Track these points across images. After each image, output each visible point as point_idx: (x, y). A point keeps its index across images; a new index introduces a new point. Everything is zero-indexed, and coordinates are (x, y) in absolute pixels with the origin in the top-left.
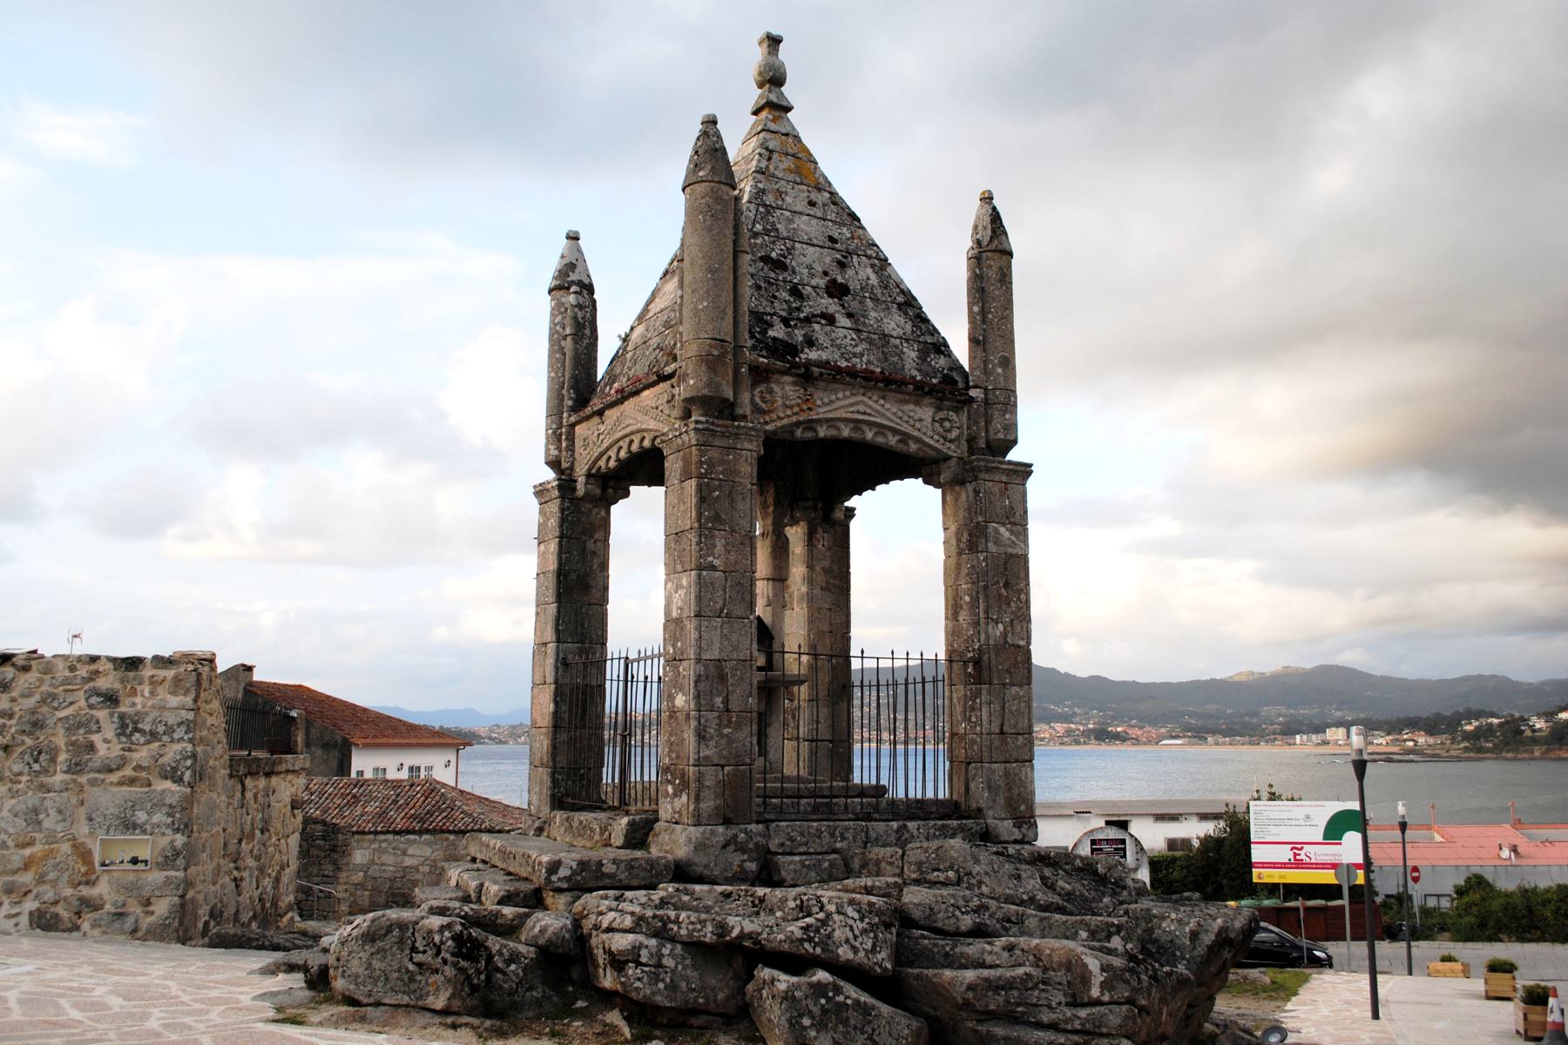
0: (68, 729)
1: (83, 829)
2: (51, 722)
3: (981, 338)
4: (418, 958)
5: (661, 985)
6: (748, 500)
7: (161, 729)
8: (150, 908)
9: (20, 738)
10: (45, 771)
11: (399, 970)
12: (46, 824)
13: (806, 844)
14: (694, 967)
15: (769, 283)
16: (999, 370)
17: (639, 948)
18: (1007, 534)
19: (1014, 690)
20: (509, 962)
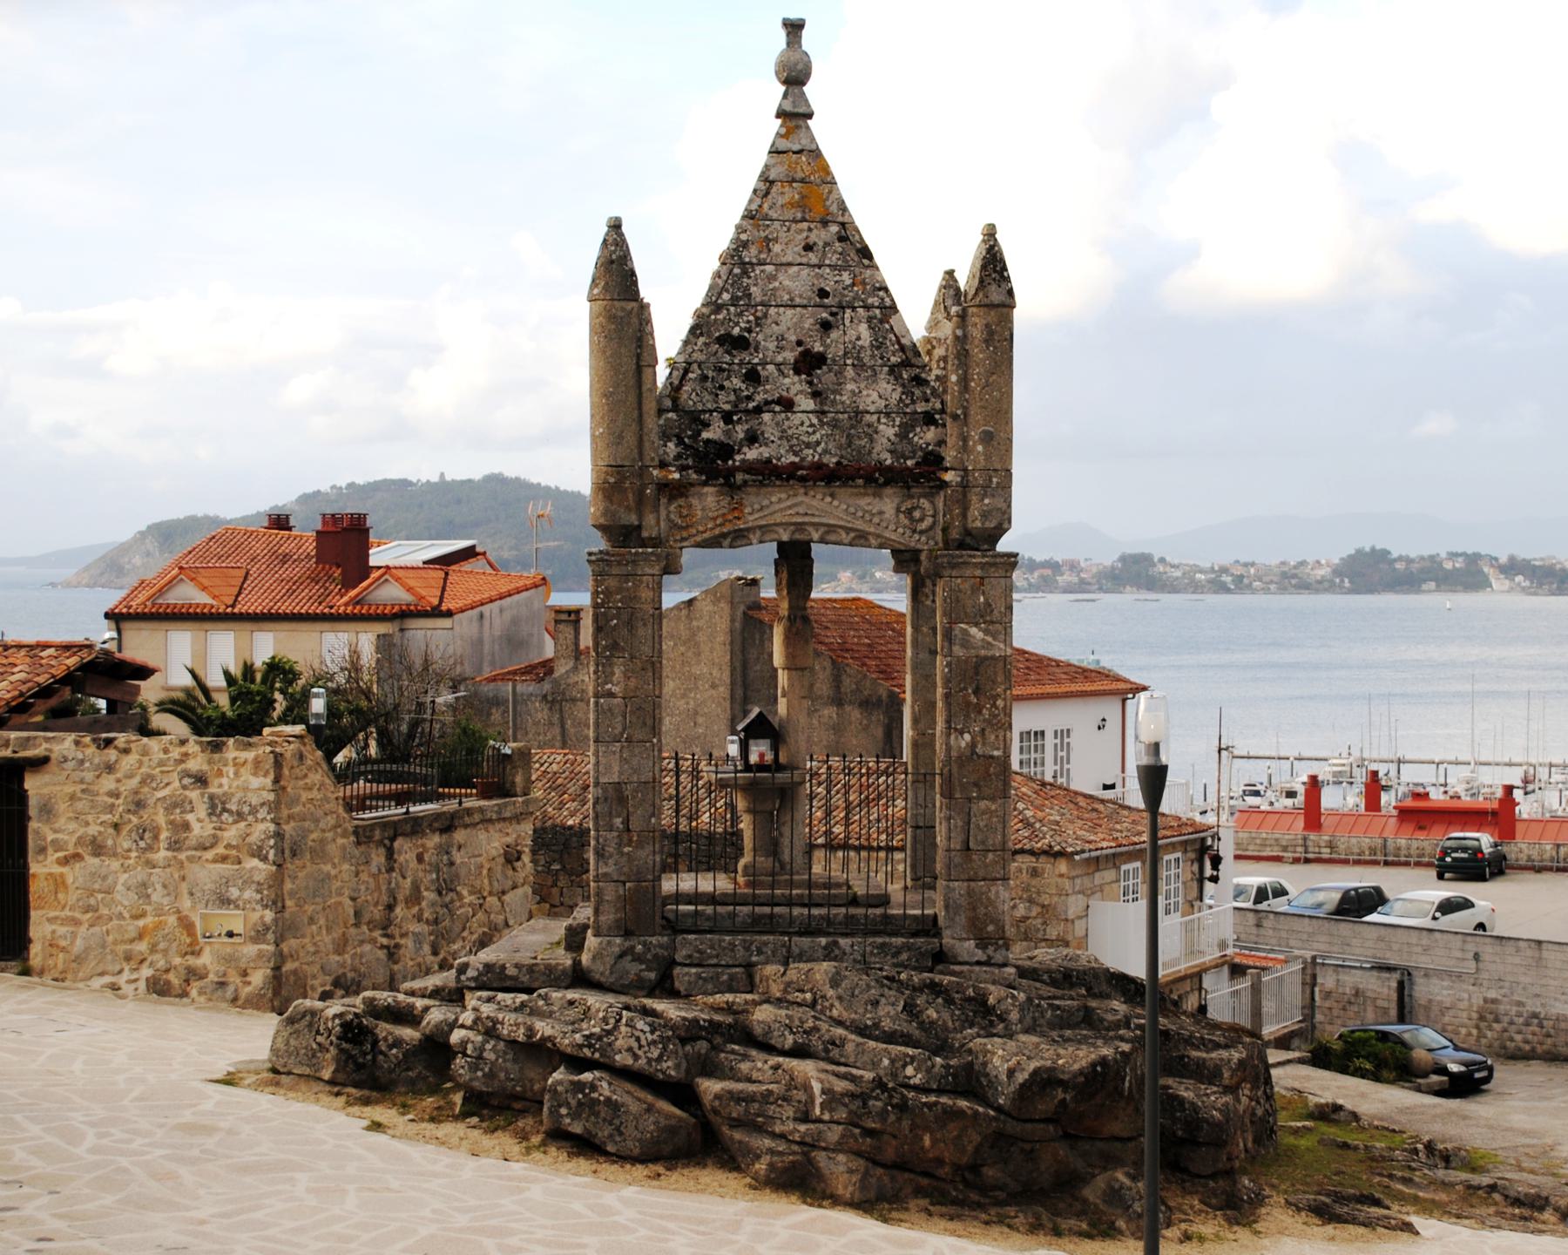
0: (166, 809)
1: (186, 903)
2: (151, 802)
3: (959, 412)
4: (319, 1039)
5: (480, 1074)
6: (650, 626)
7: (246, 809)
8: (248, 979)
9: (127, 816)
10: (149, 848)
11: (306, 1048)
12: (155, 898)
13: (717, 956)
14: (515, 1061)
15: (721, 370)
16: (980, 448)
17: (467, 1042)
18: (980, 635)
19: (983, 804)
20: (391, 1047)
